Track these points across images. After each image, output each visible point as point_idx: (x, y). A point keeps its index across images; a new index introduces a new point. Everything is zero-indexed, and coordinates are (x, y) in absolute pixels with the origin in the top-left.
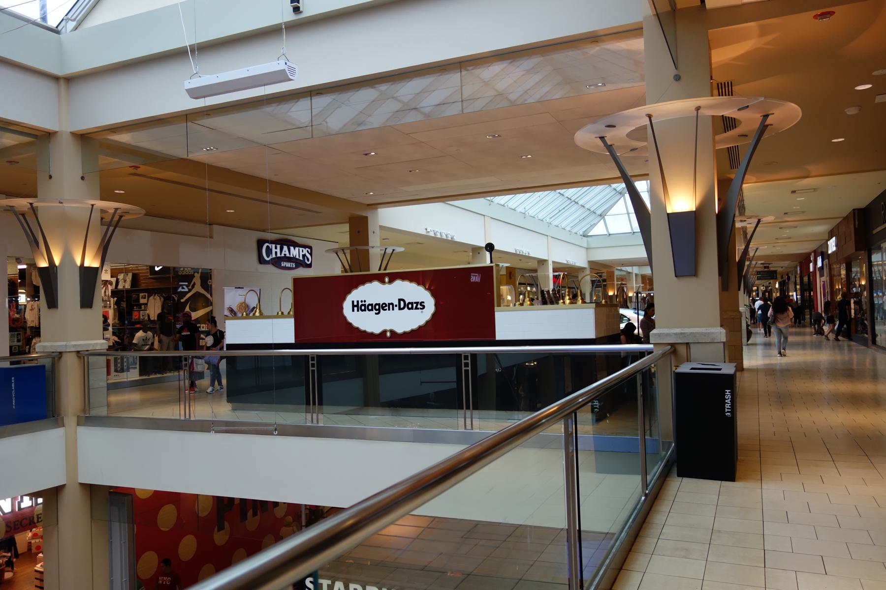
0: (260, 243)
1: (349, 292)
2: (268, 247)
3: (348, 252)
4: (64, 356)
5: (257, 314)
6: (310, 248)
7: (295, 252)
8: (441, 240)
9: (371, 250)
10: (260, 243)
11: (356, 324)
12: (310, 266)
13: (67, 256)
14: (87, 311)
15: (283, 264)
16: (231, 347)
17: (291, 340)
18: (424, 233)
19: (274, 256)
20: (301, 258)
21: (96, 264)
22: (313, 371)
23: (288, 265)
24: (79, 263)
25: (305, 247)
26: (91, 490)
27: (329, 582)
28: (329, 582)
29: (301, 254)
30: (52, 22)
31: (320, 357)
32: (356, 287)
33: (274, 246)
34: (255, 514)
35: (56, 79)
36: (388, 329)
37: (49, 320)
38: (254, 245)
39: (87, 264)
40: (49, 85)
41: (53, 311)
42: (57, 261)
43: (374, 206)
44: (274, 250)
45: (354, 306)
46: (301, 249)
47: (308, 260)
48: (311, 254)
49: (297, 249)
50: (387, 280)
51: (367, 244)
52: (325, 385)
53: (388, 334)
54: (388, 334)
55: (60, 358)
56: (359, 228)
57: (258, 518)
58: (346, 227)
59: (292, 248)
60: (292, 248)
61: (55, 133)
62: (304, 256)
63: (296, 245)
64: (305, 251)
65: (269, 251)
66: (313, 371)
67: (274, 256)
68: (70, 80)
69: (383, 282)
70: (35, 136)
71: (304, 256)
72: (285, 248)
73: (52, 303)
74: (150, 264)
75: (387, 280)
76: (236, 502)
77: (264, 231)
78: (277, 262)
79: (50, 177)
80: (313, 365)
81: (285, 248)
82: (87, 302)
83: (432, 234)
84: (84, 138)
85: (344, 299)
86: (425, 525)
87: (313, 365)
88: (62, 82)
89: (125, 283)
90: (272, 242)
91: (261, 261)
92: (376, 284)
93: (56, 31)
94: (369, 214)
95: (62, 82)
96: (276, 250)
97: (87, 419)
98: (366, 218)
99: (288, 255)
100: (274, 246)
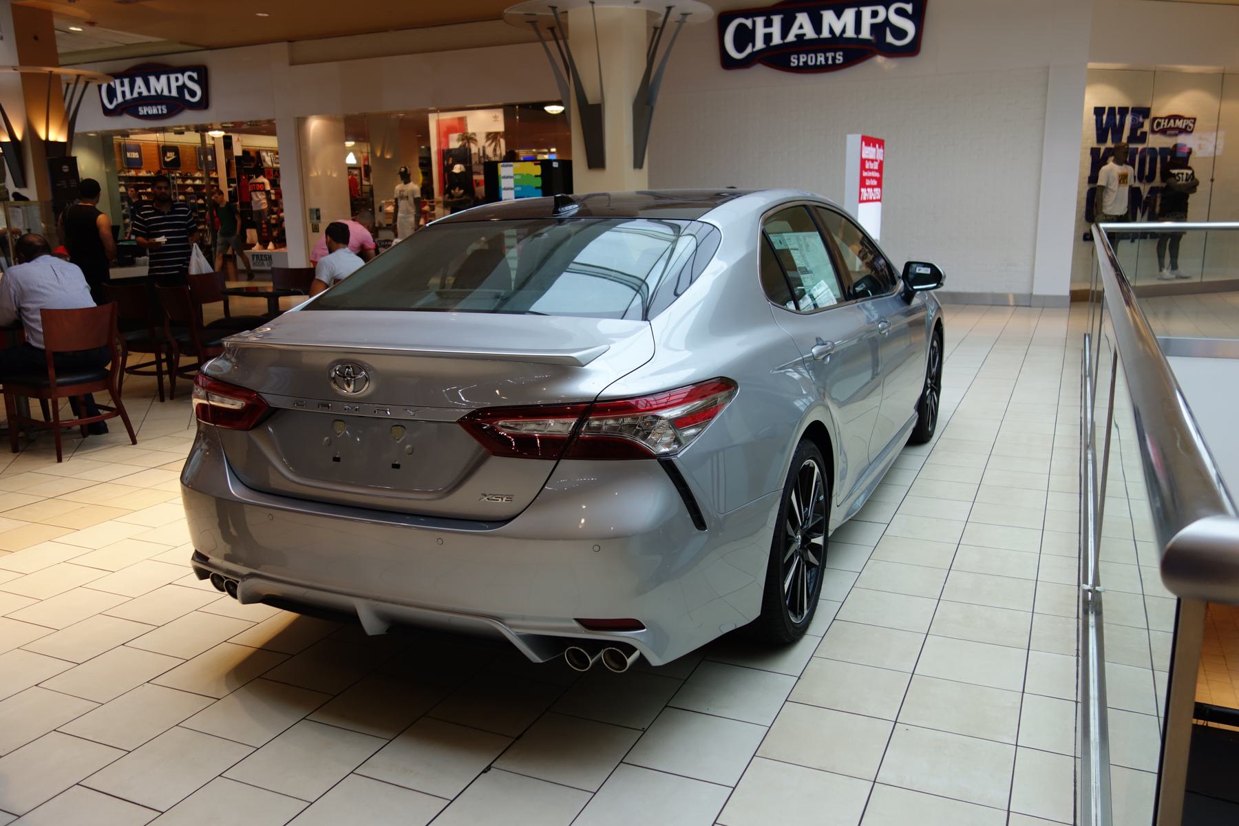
2: (741, 27)
13: (30, 130)
14: (637, 171)
15: (143, 111)
19: (120, 99)
20: (174, 93)
21: (62, 138)
23: (153, 110)
29: (174, 85)
33: (118, 82)
39: (52, 138)
42: (19, 136)
44: (119, 90)
46: (173, 77)
47: (193, 94)
49: (163, 78)
59: (152, 79)
60: (152, 79)
64: (184, 79)
65: (744, 37)
67: (120, 99)
72: (139, 82)
78: (777, 58)
86: (540, 44)
89: (268, 159)
90: (116, 76)
96: (123, 91)
99: (145, 93)
100: (760, 21)
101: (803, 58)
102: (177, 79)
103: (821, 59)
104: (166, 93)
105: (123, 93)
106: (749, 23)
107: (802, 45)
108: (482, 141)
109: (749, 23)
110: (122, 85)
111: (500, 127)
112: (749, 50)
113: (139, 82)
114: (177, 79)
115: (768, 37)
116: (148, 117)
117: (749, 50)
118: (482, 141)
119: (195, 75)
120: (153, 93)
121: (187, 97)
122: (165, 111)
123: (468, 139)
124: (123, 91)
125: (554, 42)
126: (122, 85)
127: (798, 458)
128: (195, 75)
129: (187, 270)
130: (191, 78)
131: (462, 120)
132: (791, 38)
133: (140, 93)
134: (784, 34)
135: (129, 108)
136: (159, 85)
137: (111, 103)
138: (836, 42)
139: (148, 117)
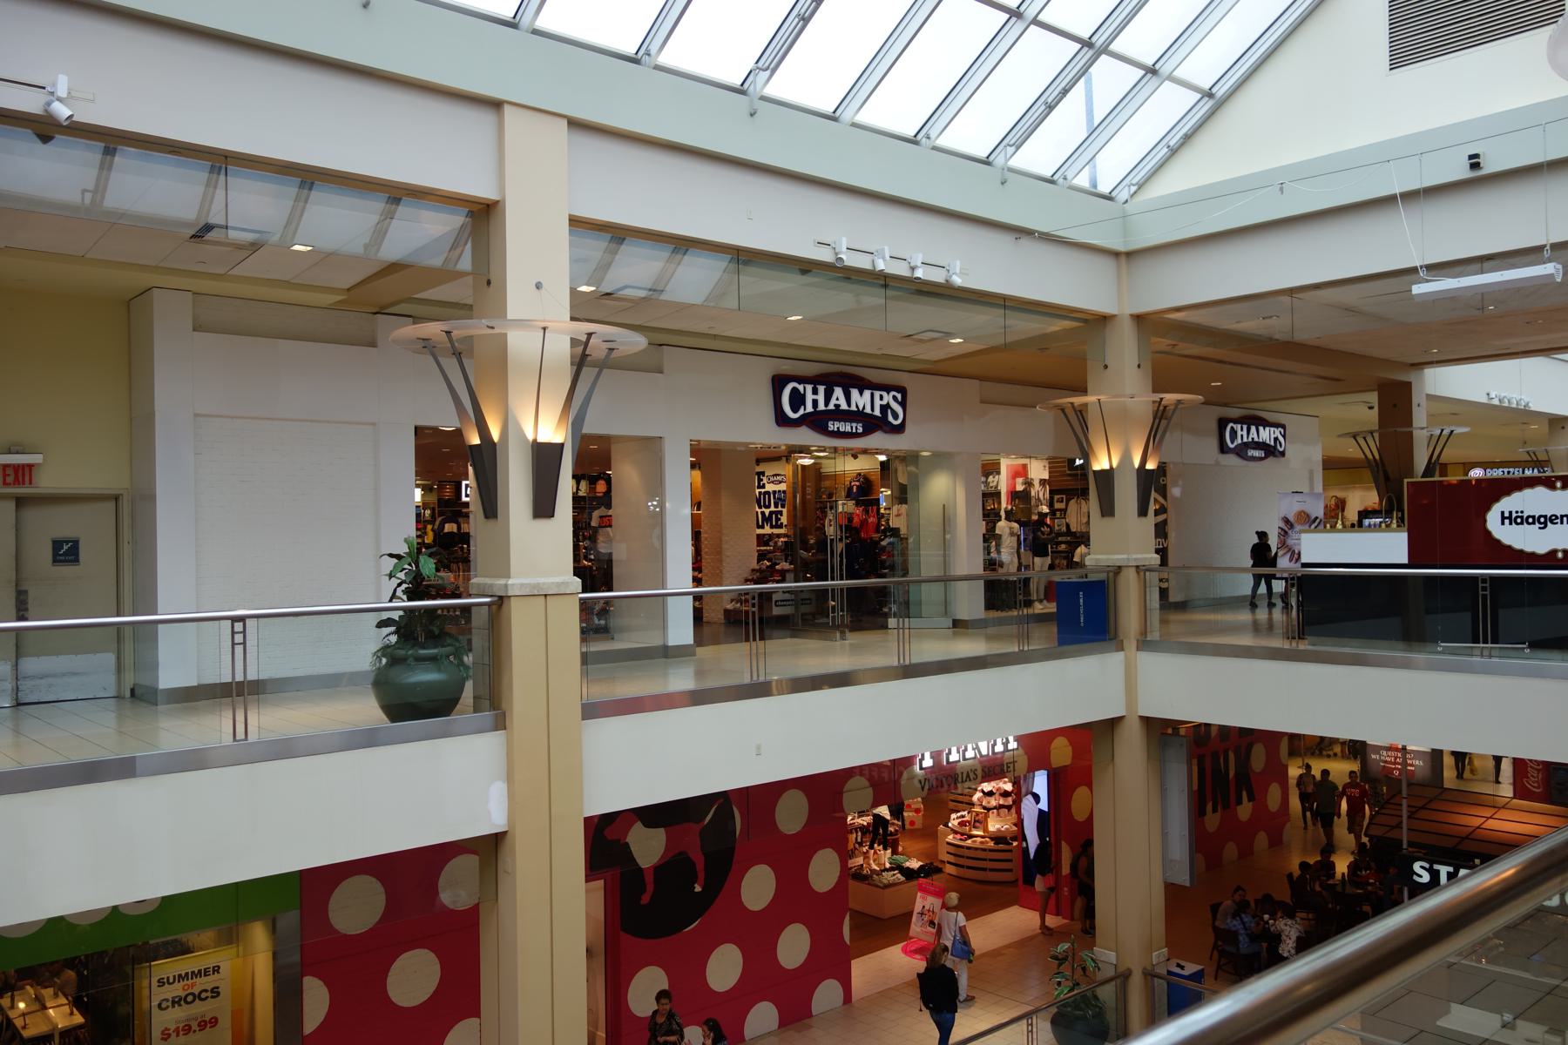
0: (1222, 423)
1: (1497, 500)
2: (794, 390)
3: (1376, 435)
4: (1124, 573)
5: (1339, 526)
6: (1283, 427)
7: (861, 400)
8: (1509, 409)
9: (1416, 433)
10: (1222, 423)
11: (1506, 541)
12: (900, 429)
14: (543, 523)
15: (833, 426)
16: (1305, 565)
17: (1405, 561)
18: (1484, 400)
19: (810, 409)
20: (877, 412)
22: (1484, 597)
23: (845, 427)
24: (1137, 463)
25: (1277, 425)
26: (1147, 721)
27: (1451, 869)
28: (1451, 869)
29: (878, 403)
30: (1104, 188)
31: (1493, 578)
32: (1508, 493)
33: (809, 388)
34: (1215, 810)
35: (1116, 254)
36: (1560, 547)
37: (1099, 528)
38: (1214, 426)
40: (1107, 264)
41: (491, 522)
42: (495, 434)
43: (1419, 366)
44: (810, 397)
45: (1503, 518)
46: (877, 394)
47: (896, 416)
48: (903, 404)
49: (867, 393)
50: (1559, 484)
51: (1410, 424)
52: (1501, 612)
53: (1560, 555)
54: (1560, 555)
55: (500, 606)
56: (1396, 401)
57: (1218, 815)
58: (1373, 398)
59: (855, 393)
60: (855, 393)
61: (1113, 316)
62: (1276, 439)
63: (863, 385)
65: (797, 400)
66: (1484, 597)
67: (810, 409)
68: (1130, 255)
69: (1552, 487)
70: (1086, 321)
71: (1276, 439)
72: (838, 392)
73: (1108, 509)
74: (1070, 456)
75: (1559, 484)
76: (1214, 732)
77: (1226, 405)
78: (1241, 451)
79: (489, 283)
80: (1484, 589)
81: (838, 392)
82: (543, 507)
83: (1496, 402)
84: (1139, 319)
85: (1488, 509)
87: (1484, 589)
88: (1123, 259)
90: (1236, 422)
91: (1223, 449)
92: (1541, 490)
93: (1108, 198)
94: (1411, 377)
95: (1123, 259)
96: (814, 399)
97: (1144, 644)
98: (1409, 384)
99: (844, 406)
100: (809, 388)
101: (837, 424)
102: (881, 398)
103: (848, 429)
104: (868, 410)
105: (815, 403)
106: (801, 387)
107: (838, 414)
108: (1036, 483)
109: (801, 387)
110: (815, 392)
111: (1046, 477)
112: (801, 412)
113: (838, 392)
114: (881, 398)
115: (815, 403)
116: (839, 434)
117: (801, 412)
118: (1036, 483)
119: (899, 396)
120: (854, 408)
121: (890, 418)
122: (860, 430)
123: (1029, 484)
124: (814, 399)
125: (454, 361)
126: (815, 392)
127: (1446, 886)
128: (899, 396)
129: (273, 929)
130: (895, 398)
131: (1025, 466)
132: (831, 407)
133: (837, 406)
134: (826, 404)
135: (817, 421)
136: (861, 400)
137: (795, 410)
138: (858, 416)
139: (839, 434)
